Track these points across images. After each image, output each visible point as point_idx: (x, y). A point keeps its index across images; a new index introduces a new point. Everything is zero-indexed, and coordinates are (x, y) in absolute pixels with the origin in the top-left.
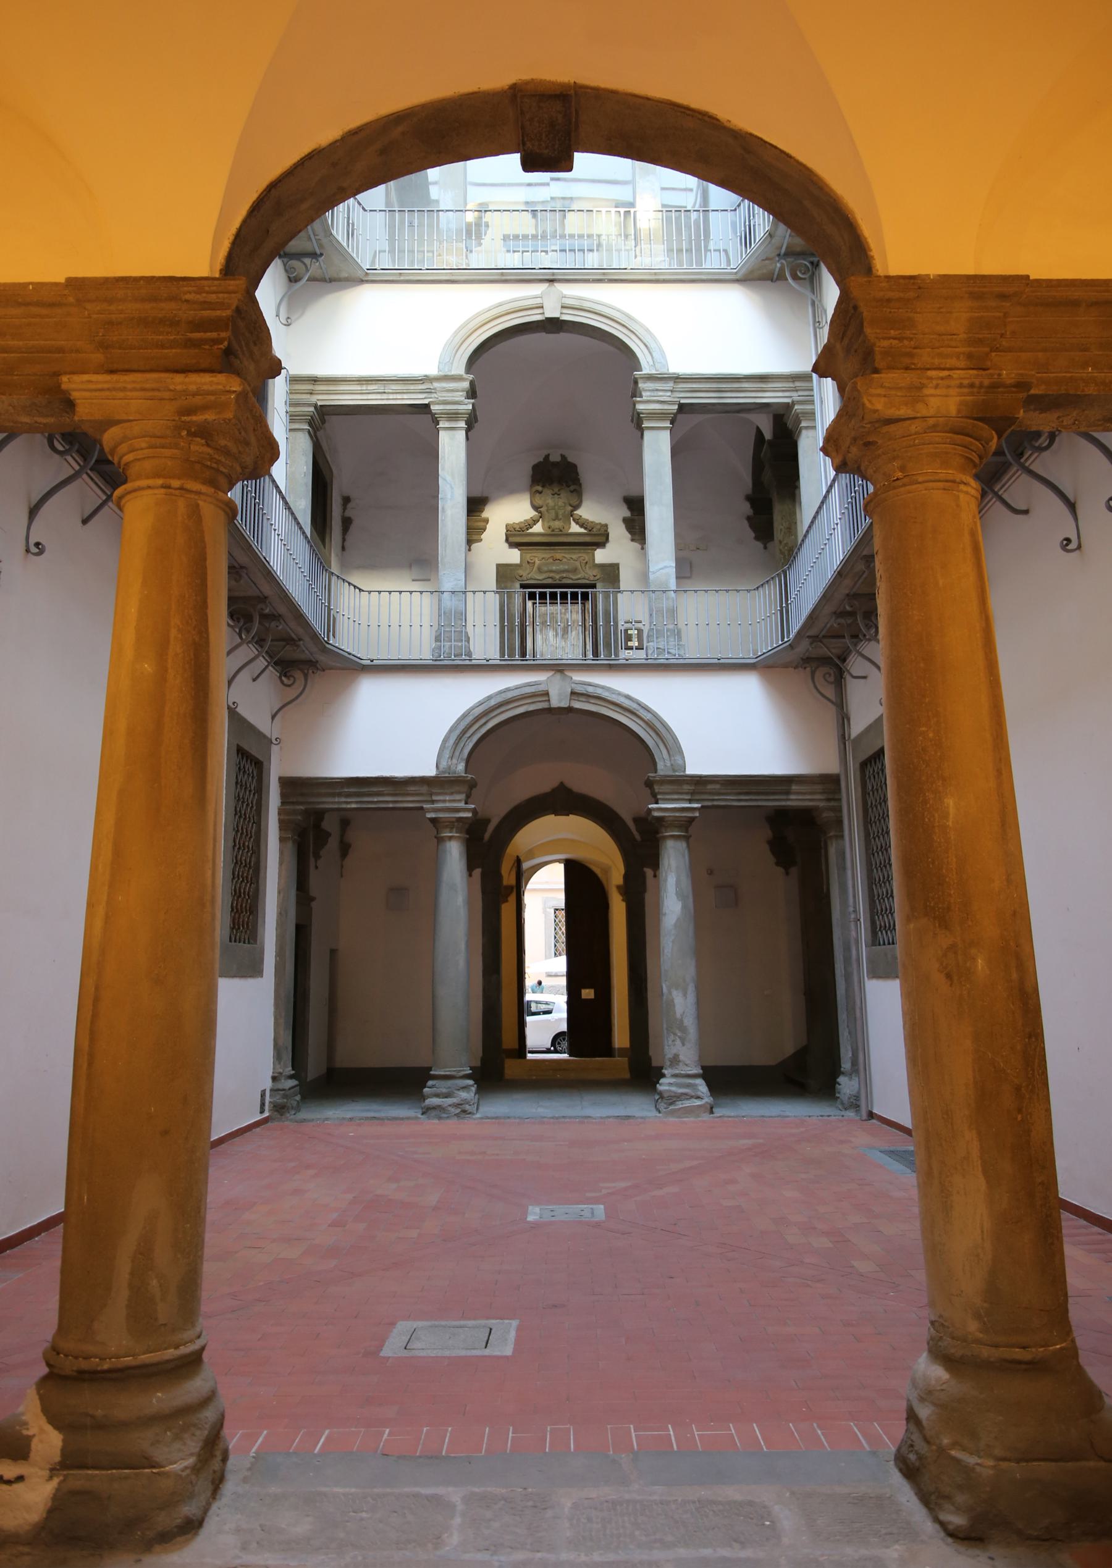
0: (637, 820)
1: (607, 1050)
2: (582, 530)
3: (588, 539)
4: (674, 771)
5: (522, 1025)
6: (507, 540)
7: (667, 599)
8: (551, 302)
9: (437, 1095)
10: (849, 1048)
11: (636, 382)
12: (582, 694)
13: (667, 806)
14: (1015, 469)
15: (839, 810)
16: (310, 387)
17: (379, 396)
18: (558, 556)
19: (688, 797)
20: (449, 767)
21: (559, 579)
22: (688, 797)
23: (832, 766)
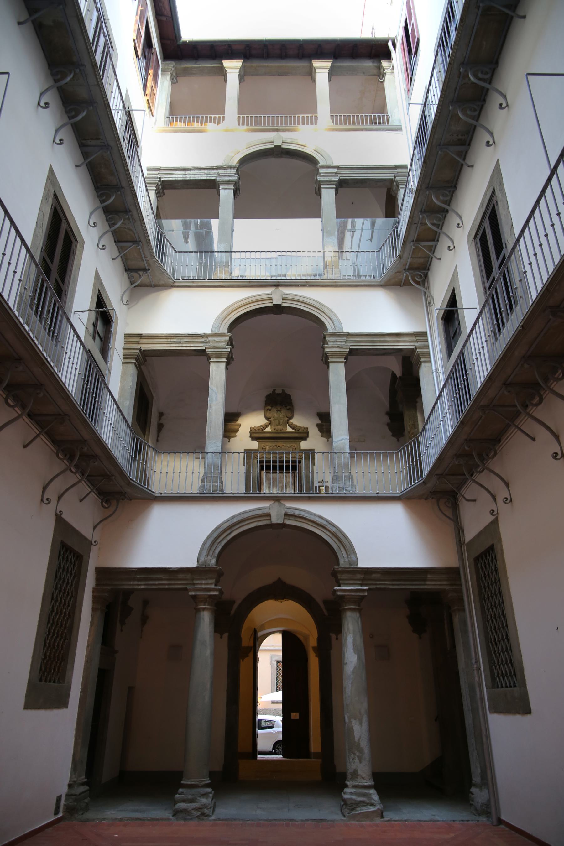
0: (325, 602)
1: (307, 754)
2: (294, 431)
3: (297, 435)
4: (350, 564)
5: (255, 736)
6: (251, 436)
7: (344, 458)
8: (277, 297)
9: (184, 801)
10: (478, 765)
11: (325, 338)
12: (292, 515)
13: (347, 588)
14: (552, 381)
15: (461, 591)
16: (138, 340)
17: (177, 345)
18: (279, 445)
19: (360, 582)
20: (206, 562)
21: (279, 461)
22: (360, 582)
23: (452, 561)
